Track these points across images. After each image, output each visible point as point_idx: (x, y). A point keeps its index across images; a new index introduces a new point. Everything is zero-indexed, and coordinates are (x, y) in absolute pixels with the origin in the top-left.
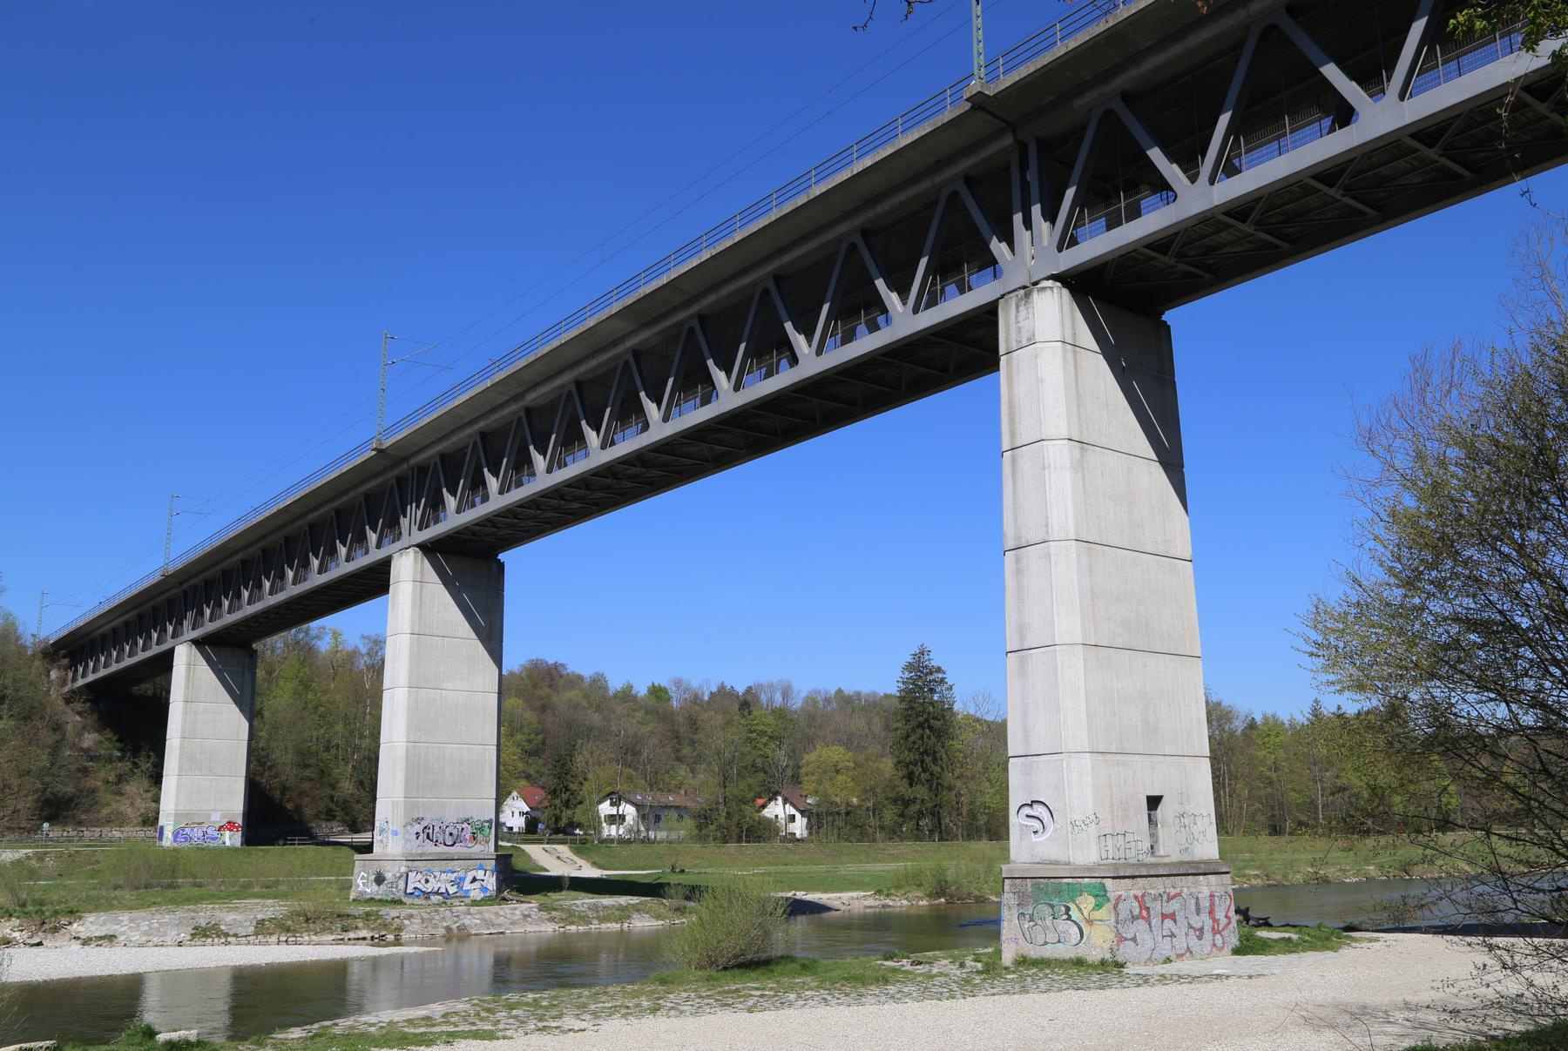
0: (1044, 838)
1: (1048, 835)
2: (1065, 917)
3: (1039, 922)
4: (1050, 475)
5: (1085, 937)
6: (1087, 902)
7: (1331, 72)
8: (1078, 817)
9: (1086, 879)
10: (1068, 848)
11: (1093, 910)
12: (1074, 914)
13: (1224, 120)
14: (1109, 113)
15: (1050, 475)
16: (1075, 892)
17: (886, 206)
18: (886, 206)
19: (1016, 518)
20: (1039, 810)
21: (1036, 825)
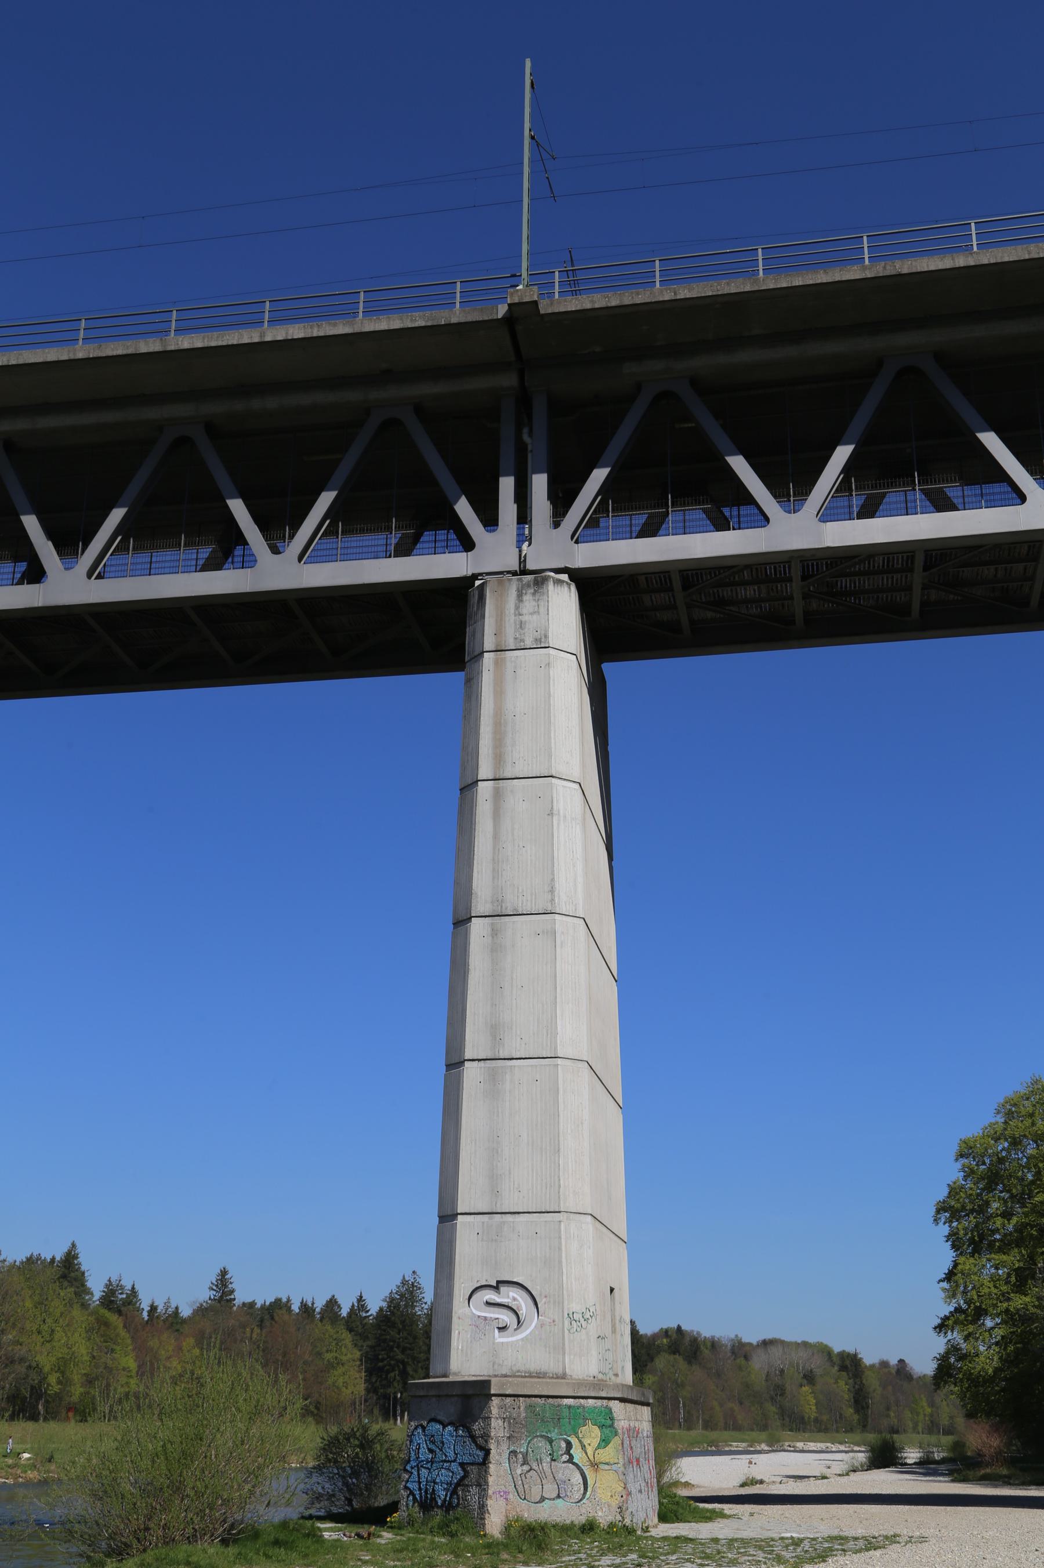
0: (514, 1339)
1: (528, 1332)
2: (565, 1458)
3: (534, 1466)
4: (558, 824)
5: (589, 1489)
6: (592, 1434)
7: (31, 523)
8: (575, 1306)
9: (590, 1401)
10: (564, 1354)
11: (598, 1447)
12: (577, 1453)
13: (117, 515)
14: (182, 442)
15: (558, 824)
16: (578, 1419)
17: (272, 403)
18: (272, 403)
19: (496, 873)
20: (511, 1294)
21: (506, 1317)
